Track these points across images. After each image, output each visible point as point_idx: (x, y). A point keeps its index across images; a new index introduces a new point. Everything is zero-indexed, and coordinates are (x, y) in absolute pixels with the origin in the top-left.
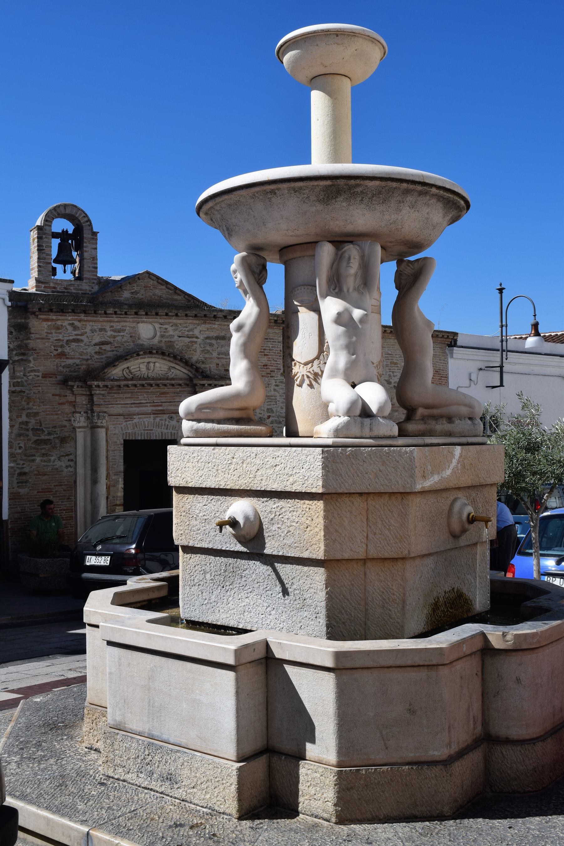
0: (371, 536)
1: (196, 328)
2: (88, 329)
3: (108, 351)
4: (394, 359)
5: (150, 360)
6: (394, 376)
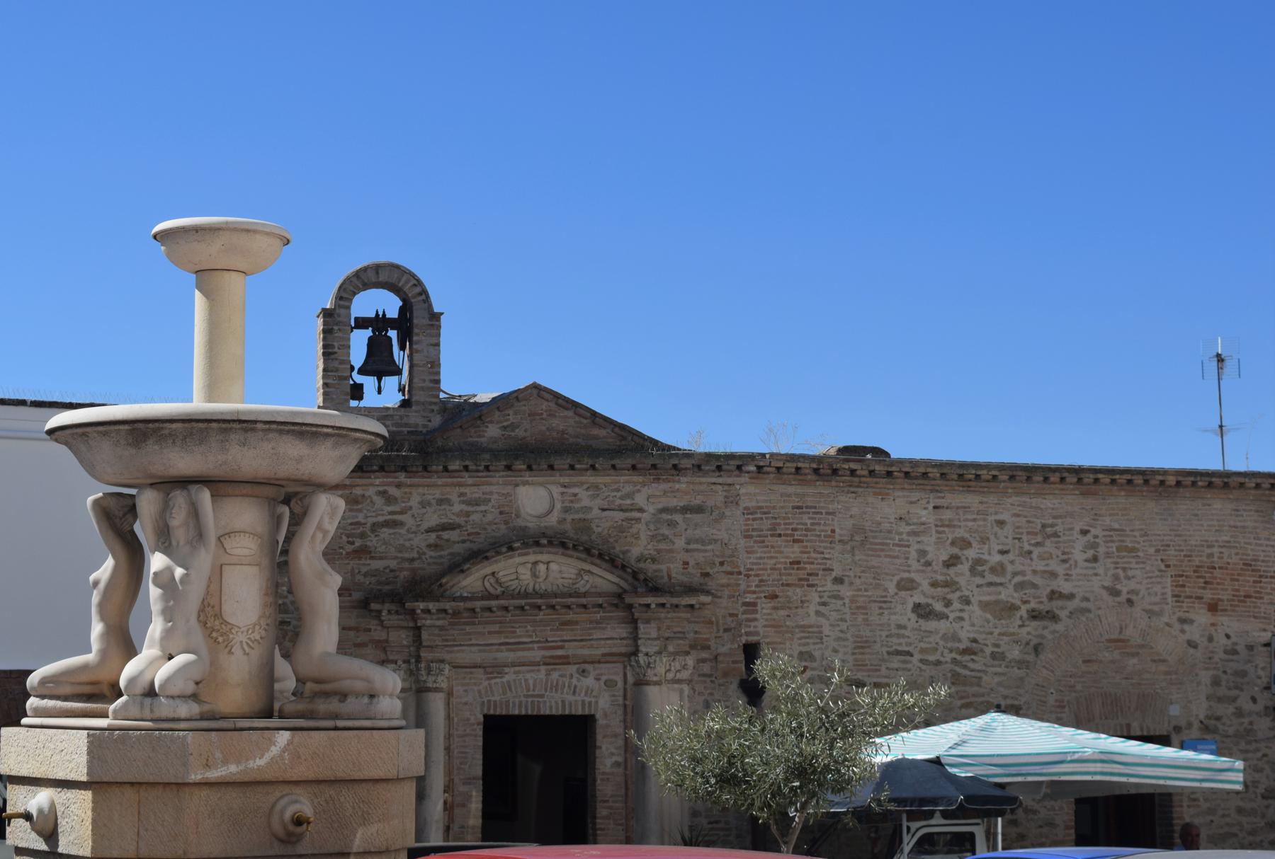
0: (142, 832)
1: (639, 491)
2: (414, 501)
3: (454, 542)
4: (1128, 539)
5: (539, 557)
6: (1129, 578)
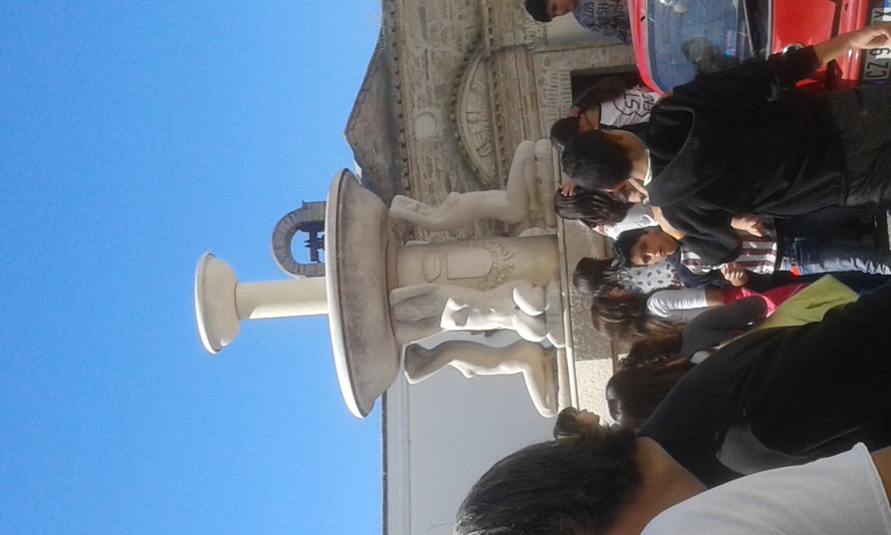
5: (464, 120)
